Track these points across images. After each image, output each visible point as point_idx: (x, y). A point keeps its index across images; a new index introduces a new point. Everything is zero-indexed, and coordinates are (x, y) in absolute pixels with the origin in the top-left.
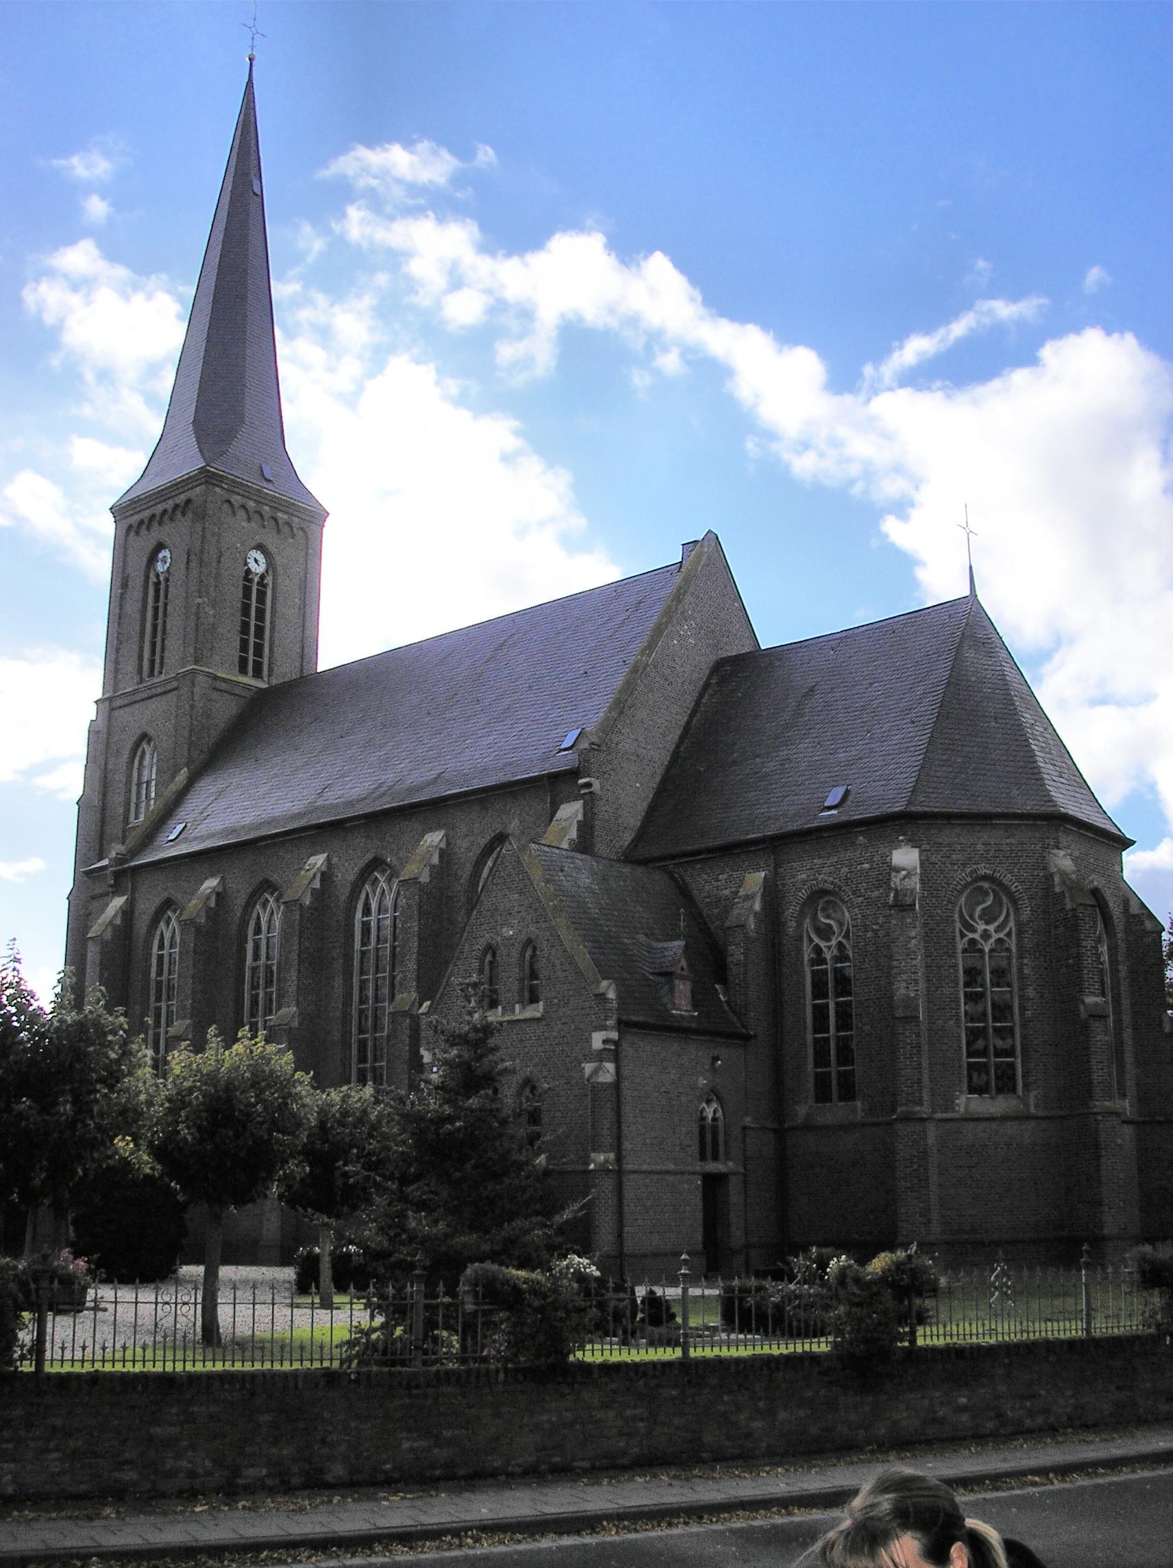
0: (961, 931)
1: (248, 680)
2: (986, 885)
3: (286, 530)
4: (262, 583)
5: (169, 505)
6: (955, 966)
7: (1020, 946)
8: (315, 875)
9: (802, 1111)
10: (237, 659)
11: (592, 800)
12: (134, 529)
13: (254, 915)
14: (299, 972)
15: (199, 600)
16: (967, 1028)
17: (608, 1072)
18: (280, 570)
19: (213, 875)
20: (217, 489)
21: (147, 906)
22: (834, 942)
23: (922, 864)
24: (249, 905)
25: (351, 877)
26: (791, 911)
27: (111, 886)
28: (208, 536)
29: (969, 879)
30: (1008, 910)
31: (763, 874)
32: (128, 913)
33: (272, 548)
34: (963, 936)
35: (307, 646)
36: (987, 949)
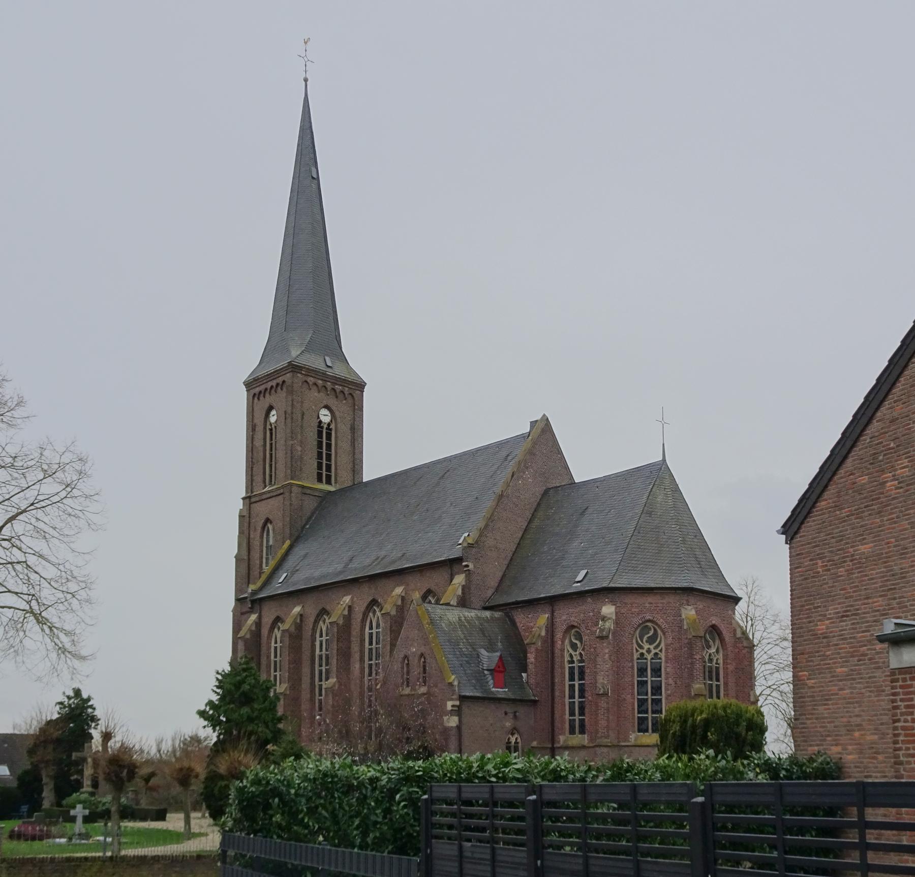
0: (636, 649)
1: (324, 487)
2: (649, 624)
3: (341, 396)
4: (329, 429)
5: (274, 383)
6: (632, 667)
7: (666, 657)
8: (344, 609)
9: (562, 739)
10: (315, 474)
11: (469, 574)
12: (257, 396)
13: (319, 627)
14: (337, 660)
15: (291, 442)
16: (638, 699)
17: (453, 722)
18: (339, 420)
19: (299, 604)
20: (299, 375)
21: (268, 620)
22: (578, 653)
23: (616, 613)
24: (316, 622)
25: (363, 609)
26: (559, 635)
27: (250, 608)
28: (295, 403)
29: (641, 622)
30: (661, 638)
31: (547, 616)
32: (258, 624)
33: (334, 408)
34: (637, 651)
35: (356, 465)
36: (649, 658)
